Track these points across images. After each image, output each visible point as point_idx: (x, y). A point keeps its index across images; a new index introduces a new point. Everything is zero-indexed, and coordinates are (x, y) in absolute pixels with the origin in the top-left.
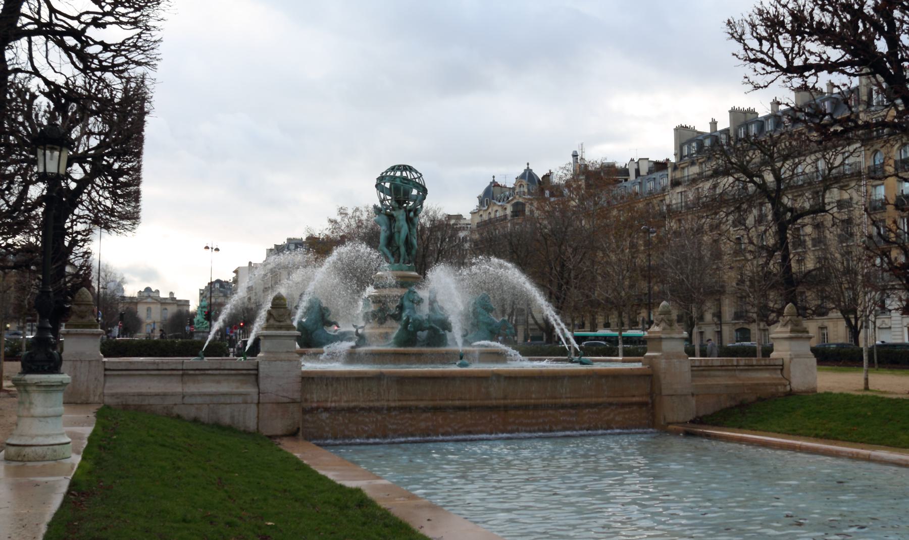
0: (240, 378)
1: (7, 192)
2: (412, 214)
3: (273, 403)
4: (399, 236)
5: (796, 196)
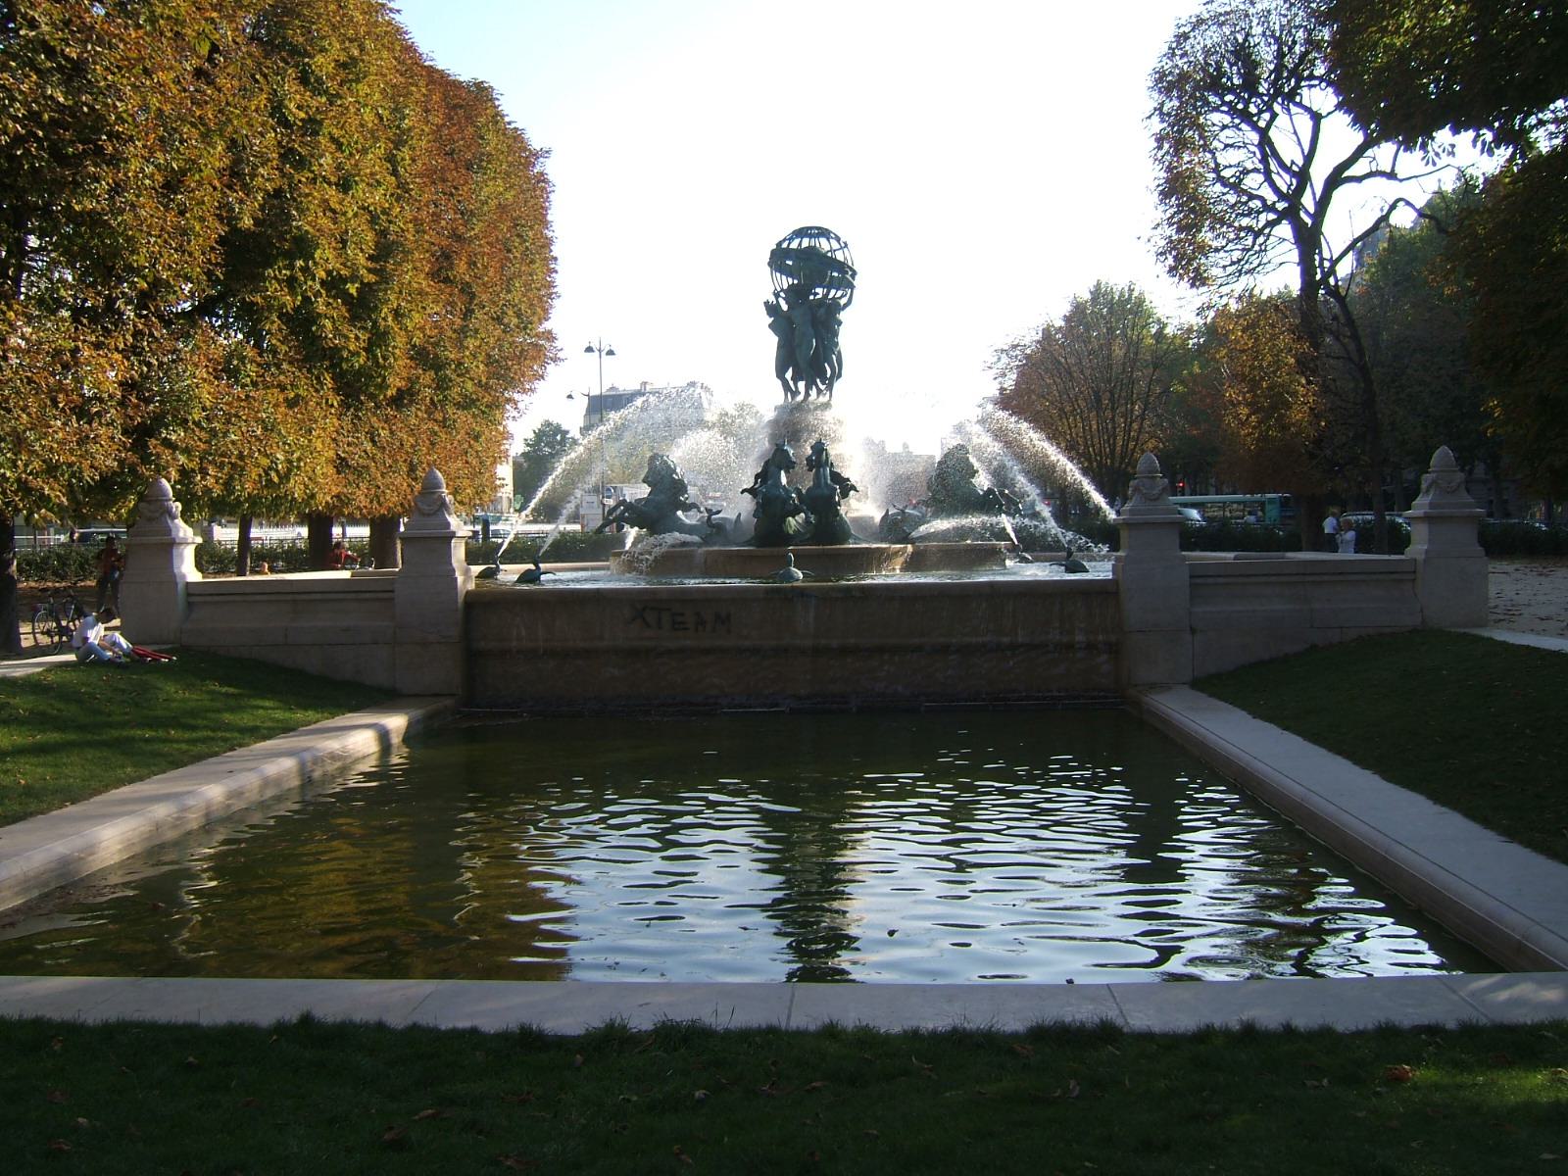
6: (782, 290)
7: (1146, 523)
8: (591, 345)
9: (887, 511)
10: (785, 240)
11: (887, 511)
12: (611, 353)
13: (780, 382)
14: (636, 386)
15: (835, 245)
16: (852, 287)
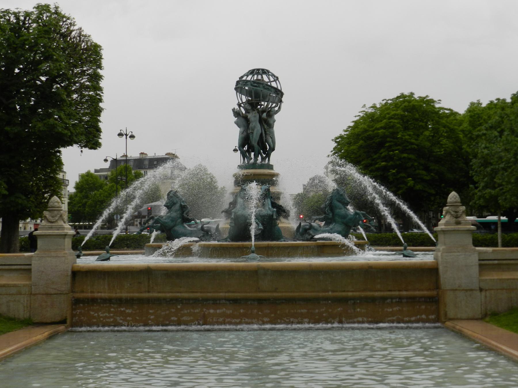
0: (433, 331)
1: (37, 19)
2: (265, 115)
3: (43, 294)
4: (253, 136)
5: (422, 121)
6: (243, 103)
7: (454, 230)
8: (122, 132)
9: (300, 224)
10: (244, 75)
11: (300, 224)
12: (132, 137)
13: (99, 169)
14: (161, 153)
15: (272, 79)
16: (281, 101)
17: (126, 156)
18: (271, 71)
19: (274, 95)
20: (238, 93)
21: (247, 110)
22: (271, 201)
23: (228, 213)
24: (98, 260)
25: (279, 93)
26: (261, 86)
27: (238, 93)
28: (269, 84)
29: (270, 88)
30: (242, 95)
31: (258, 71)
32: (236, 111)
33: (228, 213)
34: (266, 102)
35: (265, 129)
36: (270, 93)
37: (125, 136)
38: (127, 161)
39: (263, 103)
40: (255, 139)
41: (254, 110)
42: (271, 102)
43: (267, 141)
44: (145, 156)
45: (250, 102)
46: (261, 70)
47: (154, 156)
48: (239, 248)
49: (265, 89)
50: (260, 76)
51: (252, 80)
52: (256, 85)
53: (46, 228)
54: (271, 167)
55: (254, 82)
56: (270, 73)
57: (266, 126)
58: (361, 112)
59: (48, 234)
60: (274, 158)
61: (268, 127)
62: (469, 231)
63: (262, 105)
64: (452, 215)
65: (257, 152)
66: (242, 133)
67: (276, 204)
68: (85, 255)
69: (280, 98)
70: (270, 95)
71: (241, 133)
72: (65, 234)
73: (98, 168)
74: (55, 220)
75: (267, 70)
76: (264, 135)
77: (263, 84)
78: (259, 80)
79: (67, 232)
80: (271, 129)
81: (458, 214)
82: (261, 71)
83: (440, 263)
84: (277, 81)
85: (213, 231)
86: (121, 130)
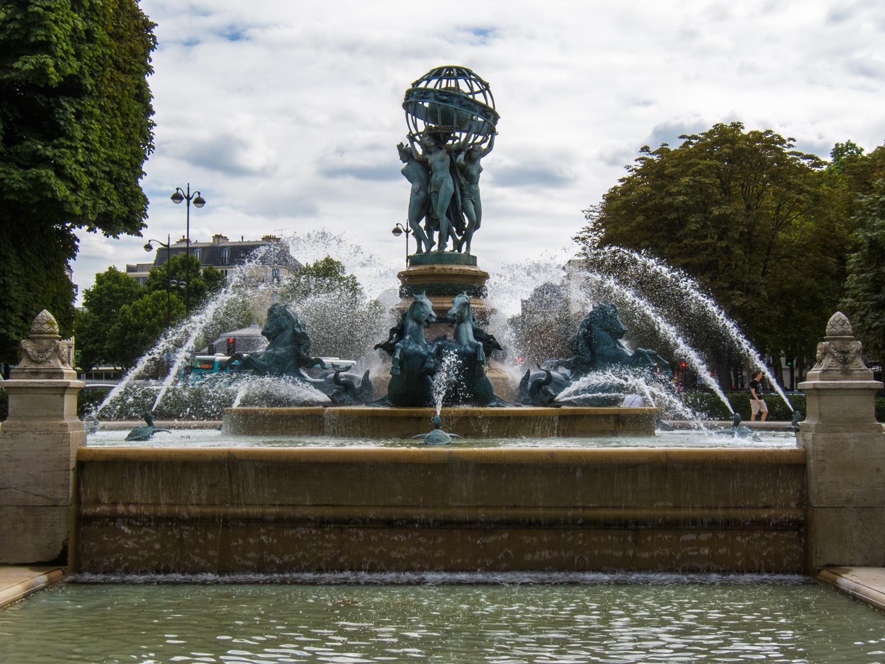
2: (461, 157)
4: (437, 200)
6: (418, 134)
9: (528, 372)
10: (422, 80)
11: (528, 372)
12: (200, 202)
16: (493, 132)
17: (188, 241)
18: (474, 71)
19: (480, 119)
20: (409, 115)
21: (427, 148)
22: (473, 326)
23: (388, 348)
24: (130, 438)
25: (490, 115)
26: (455, 100)
27: (409, 115)
28: (471, 97)
29: (472, 104)
30: (418, 119)
31: (450, 72)
32: (406, 150)
33: (388, 348)
34: (465, 132)
35: (461, 186)
36: (473, 116)
37: (185, 201)
38: (190, 250)
39: (457, 134)
40: (442, 202)
41: (441, 149)
42: (475, 133)
43: (465, 209)
44: (224, 241)
45: (432, 132)
46: (455, 70)
47: (240, 242)
48: (409, 418)
49: (463, 106)
50: (453, 81)
51: (438, 88)
52: (445, 98)
53: (27, 373)
54: (473, 261)
55: (441, 92)
56: (472, 76)
57: (463, 180)
58: (640, 159)
59: (30, 385)
60: (478, 245)
61: (468, 183)
62: (868, 389)
63: (456, 138)
64: (834, 357)
65: (444, 230)
66: (417, 193)
67: (481, 332)
68: (103, 428)
69: (492, 125)
70: (472, 119)
71: (414, 193)
72: (65, 385)
73: (134, 264)
74: (44, 359)
75: (467, 70)
76: (459, 197)
77: (459, 97)
78: (451, 88)
79: (69, 383)
80: (473, 187)
81: (847, 356)
82: (455, 72)
83: (810, 453)
84: (487, 92)
85: (357, 386)
86: (177, 189)
